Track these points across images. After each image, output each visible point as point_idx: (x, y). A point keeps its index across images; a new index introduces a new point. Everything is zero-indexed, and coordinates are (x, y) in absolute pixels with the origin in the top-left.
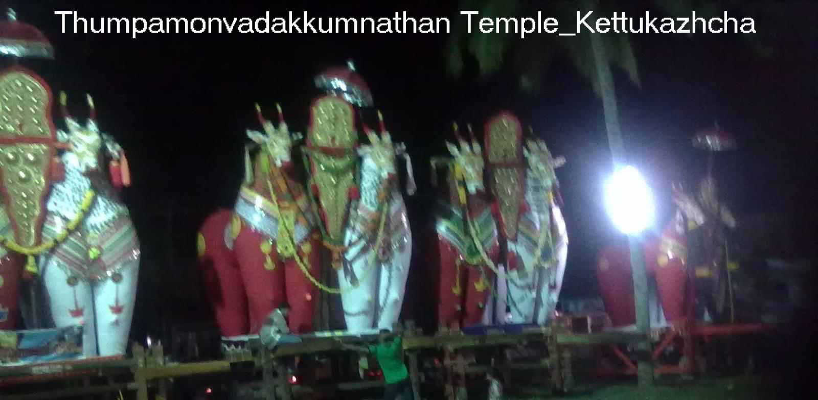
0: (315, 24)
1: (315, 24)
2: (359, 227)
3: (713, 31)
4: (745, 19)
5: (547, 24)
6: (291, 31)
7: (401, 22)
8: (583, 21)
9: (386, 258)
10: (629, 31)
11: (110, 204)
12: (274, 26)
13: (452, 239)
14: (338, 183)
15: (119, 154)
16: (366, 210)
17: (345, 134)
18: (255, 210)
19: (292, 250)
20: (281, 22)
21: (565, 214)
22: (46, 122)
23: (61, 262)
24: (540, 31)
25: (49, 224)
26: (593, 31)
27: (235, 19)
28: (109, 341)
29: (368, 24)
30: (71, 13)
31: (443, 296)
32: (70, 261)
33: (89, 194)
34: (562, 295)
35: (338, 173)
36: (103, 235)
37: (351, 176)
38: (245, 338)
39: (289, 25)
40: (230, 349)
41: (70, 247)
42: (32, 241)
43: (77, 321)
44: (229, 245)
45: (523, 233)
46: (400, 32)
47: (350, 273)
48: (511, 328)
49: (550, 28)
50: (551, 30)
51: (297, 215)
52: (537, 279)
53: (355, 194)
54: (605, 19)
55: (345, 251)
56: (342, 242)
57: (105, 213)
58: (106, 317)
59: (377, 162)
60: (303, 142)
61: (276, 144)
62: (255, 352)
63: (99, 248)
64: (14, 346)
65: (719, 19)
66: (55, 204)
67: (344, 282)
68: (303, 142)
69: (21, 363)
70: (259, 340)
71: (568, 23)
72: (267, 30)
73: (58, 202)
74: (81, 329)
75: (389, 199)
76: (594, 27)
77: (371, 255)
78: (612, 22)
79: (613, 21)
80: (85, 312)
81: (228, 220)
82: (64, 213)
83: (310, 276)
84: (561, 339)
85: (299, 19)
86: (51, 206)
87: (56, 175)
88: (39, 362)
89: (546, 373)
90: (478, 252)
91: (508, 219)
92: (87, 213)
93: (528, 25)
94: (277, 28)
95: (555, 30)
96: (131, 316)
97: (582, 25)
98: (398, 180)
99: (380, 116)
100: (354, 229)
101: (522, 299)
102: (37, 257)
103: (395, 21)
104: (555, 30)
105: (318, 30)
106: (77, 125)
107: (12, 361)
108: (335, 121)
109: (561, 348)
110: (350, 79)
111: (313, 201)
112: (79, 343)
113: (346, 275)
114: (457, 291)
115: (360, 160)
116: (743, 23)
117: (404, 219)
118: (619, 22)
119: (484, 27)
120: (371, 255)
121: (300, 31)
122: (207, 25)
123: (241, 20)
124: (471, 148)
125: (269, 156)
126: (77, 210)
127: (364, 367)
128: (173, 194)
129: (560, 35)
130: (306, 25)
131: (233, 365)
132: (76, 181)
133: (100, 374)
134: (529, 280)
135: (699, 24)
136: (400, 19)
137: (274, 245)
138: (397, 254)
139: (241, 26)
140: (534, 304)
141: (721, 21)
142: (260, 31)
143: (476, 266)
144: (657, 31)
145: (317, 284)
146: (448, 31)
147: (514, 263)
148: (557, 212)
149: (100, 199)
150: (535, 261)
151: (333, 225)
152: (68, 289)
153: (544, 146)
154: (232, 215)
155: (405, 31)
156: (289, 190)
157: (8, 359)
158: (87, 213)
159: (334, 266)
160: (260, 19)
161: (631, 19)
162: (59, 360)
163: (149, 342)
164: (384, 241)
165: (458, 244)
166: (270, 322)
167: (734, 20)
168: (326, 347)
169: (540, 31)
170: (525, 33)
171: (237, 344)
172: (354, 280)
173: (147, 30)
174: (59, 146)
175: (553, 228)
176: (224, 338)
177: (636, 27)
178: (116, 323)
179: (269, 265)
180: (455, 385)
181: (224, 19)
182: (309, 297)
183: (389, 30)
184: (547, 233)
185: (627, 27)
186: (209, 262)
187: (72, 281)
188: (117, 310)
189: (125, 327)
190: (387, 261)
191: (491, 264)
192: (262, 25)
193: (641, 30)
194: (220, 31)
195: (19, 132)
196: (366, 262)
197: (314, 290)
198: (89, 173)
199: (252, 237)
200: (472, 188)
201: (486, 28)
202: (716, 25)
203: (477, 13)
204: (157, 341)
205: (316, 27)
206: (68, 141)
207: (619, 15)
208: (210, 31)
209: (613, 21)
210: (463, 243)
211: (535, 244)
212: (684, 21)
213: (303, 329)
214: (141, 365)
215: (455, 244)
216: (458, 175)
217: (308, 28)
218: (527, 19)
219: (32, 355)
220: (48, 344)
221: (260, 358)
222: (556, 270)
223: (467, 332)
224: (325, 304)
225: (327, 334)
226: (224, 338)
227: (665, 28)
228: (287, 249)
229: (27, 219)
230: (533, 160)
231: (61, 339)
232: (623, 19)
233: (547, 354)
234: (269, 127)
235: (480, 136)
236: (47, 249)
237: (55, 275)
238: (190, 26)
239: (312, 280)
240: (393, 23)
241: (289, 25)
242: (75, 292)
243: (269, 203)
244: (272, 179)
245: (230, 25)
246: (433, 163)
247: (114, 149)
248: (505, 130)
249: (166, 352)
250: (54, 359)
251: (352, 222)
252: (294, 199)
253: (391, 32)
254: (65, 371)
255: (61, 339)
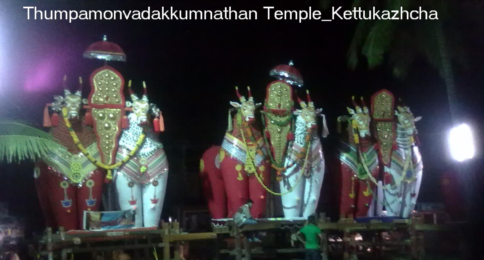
0: (177, 14)
1: (177, 14)
2: (293, 157)
3: (413, 19)
4: (432, 11)
5: (315, 15)
6: (163, 18)
7: (228, 13)
8: (336, 12)
9: (309, 174)
10: (363, 18)
11: (153, 141)
12: (153, 15)
13: (349, 164)
14: (282, 130)
15: (159, 113)
16: (297, 147)
17: (286, 103)
18: (233, 147)
19: (253, 170)
20: (157, 13)
21: (421, 151)
22: (120, 96)
23: (125, 174)
24: (310, 18)
25: (120, 153)
26: (342, 19)
27: (130, 11)
28: (149, 219)
29: (208, 14)
30: (33, 7)
31: (343, 199)
32: (129, 173)
33: (142, 136)
34: (419, 200)
35: (281, 125)
36: (149, 159)
37: (289, 127)
38: (225, 220)
39: (162, 15)
40: (216, 226)
41: (132, 166)
42: (110, 162)
43: (133, 207)
44: (218, 166)
45: (394, 162)
46: (227, 19)
47: (287, 183)
48: (385, 219)
49: (316, 16)
50: (317, 18)
51: (257, 149)
52: (403, 189)
53: (291, 138)
54: (349, 11)
55: (285, 171)
56: (283, 166)
57: (150, 147)
58: (148, 205)
59: (305, 119)
60: (261, 108)
61: (246, 109)
62: (230, 228)
63: (146, 166)
64: (99, 221)
65: (416, 11)
66: (124, 142)
67: (283, 189)
68: (261, 108)
69: (102, 230)
70: (233, 221)
71: (327, 14)
72: (149, 18)
73: (126, 141)
74: (135, 212)
75: (311, 140)
76: (342, 16)
77: (300, 173)
78: (353, 13)
79: (354, 12)
80: (137, 202)
81: (218, 152)
82: (128, 146)
83: (263, 184)
84: (418, 227)
85: (168, 11)
86: (121, 143)
87: (124, 126)
88: (111, 229)
89: (407, 247)
90: (366, 173)
91: (385, 153)
92: (140, 147)
93: (303, 15)
94: (155, 17)
95: (320, 18)
96: (162, 205)
97: (335, 15)
98: (317, 129)
99: (308, 92)
100: (290, 157)
101: (393, 202)
102: (112, 171)
103: (224, 12)
104: (320, 18)
105: (179, 18)
106: (137, 98)
107: (97, 229)
108: (280, 95)
109: (418, 233)
110: (290, 71)
111: (267, 142)
112: (134, 220)
113: (285, 185)
114: (352, 196)
115: (295, 117)
116: (431, 14)
117: (320, 152)
118: (357, 13)
119: (277, 16)
120: (300, 173)
121: (168, 18)
122: (113, 15)
123: (134, 12)
124: (363, 110)
125: (242, 114)
126: (135, 145)
127: (295, 240)
128: (188, 136)
129: (322, 20)
130: (172, 15)
131: (218, 235)
132: (135, 128)
133: (144, 237)
134: (398, 190)
135: (405, 14)
136: (228, 11)
137: (243, 166)
138: (315, 173)
139: (133, 15)
140: (400, 205)
141: (418, 12)
142: (144, 19)
143: (364, 181)
144: (379, 18)
145: (267, 189)
146: (256, 18)
147: (389, 180)
148: (416, 149)
149: (147, 139)
150: (402, 178)
151: (278, 155)
152: (129, 189)
153: (408, 109)
154: (220, 149)
155: (230, 18)
156: (253, 135)
157: (94, 227)
158: (140, 147)
159: (277, 179)
160: (144, 11)
161: (364, 11)
162: (122, 229)
163: (170, 220)
164: (308, 165)
165: (353, 167)
166: (241, 212)
167: (426, 12)
168: (272, 227)
169: (310, 18)
170: (301, 19)
171: (220, 223)
172: (289, 188)
173: (78, 18)
174: (126, 109)
175: (413, 159)
176: (213, 219)
177: (367, 16)
178: (154, 209)
179: (240, 178)
180: (350, 253)
181: (124, 11)
182: (262, 197)
183: (221, 18)
184: (410, 161)
185: (362, 16)
186: (206, 176)
187: (131, 185)
188: (155, 201)
189: (159, 211)
190: (310, 177)
191: (374, 180)
192: (146, 15)
193: (370, 18)
194: (121, 18)
195: (106, 102)
196: (297, 178)
197: (265, 193)
198: (142, 125)
199: (231, 162)
200: (363, 134)
201: (278, 16)
202: (415, 15)
203: (273, 7)
204: (175, 219)
205: (178, 16)
206: (131, 107)
207: (357, 9)
208: (115, 18)
209: (354, 12)
210: (356, 167)
211: (402, 168)
212: (395, 13)
213: (260, 216)
214: (167, 233)
215: (352, 168)
216: (354, 127)
217: (173, 16)
218: (303, 11)
219: (106, 225)
220: (117, 220)
221: (233, 231)
222: (415, 185)
223: (359, 221)
224: (272, 201)
225: (273, 219)
226: (213, 219)
227: (385, 17)
228: (250, 169)
229: (108, 150)
230: (401, 117)
231: (124, 217)
232: (360, 11)
233: (408, 236)
234: (243, 99)
235: (368, 103)
236: (118, 166)
237: (122, 180)
238: (103, 15)
239: (265, 187)
240: (224, 13)
241: (162, 15)
242: (132, 191)
243: (240, 142)
244: (243, 128)
245: (127, 15)
246: (339, 119)
247: (156, 111)
248: (384, 100)
249: (181, 226)
250: (120, 228)
251: (289, 154)
252: (256, 140)
253: (222, 19)
254: (125, 235)
255: (124, 217)
